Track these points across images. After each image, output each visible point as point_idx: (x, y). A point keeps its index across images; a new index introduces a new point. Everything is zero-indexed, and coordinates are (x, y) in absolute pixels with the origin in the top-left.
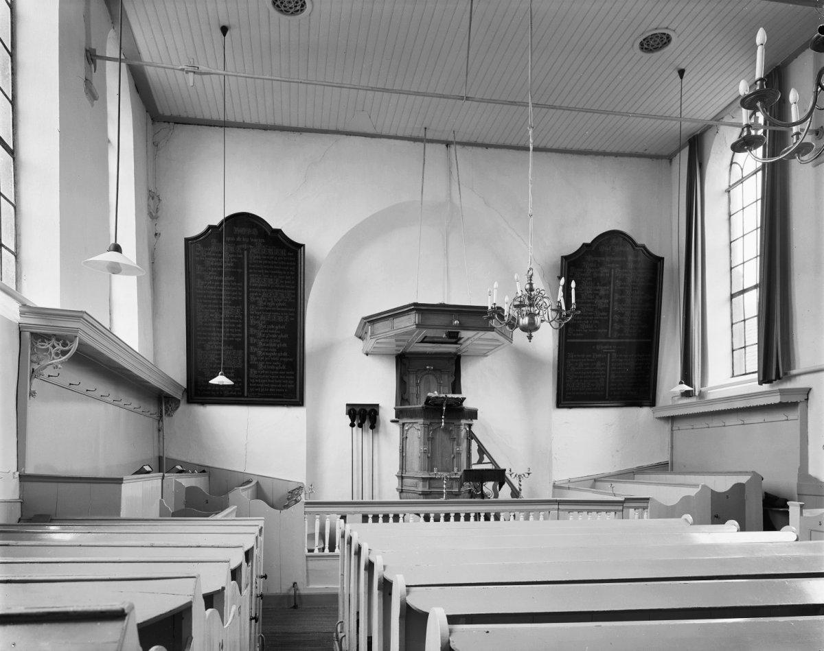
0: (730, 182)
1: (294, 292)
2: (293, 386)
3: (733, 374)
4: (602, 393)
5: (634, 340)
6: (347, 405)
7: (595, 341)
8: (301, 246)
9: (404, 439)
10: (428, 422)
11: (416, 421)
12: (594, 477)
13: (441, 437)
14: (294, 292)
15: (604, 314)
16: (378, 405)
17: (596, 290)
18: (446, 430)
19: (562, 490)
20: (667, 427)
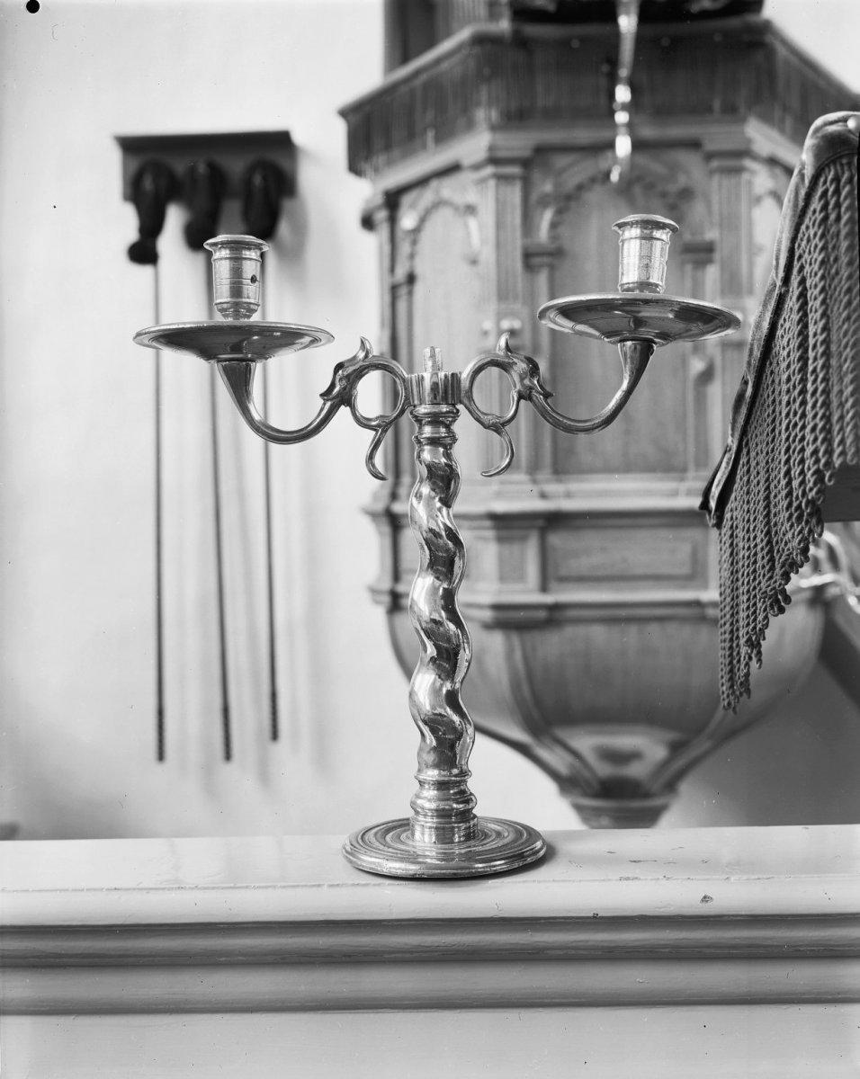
6: (131, 146)
10: (520, 142)
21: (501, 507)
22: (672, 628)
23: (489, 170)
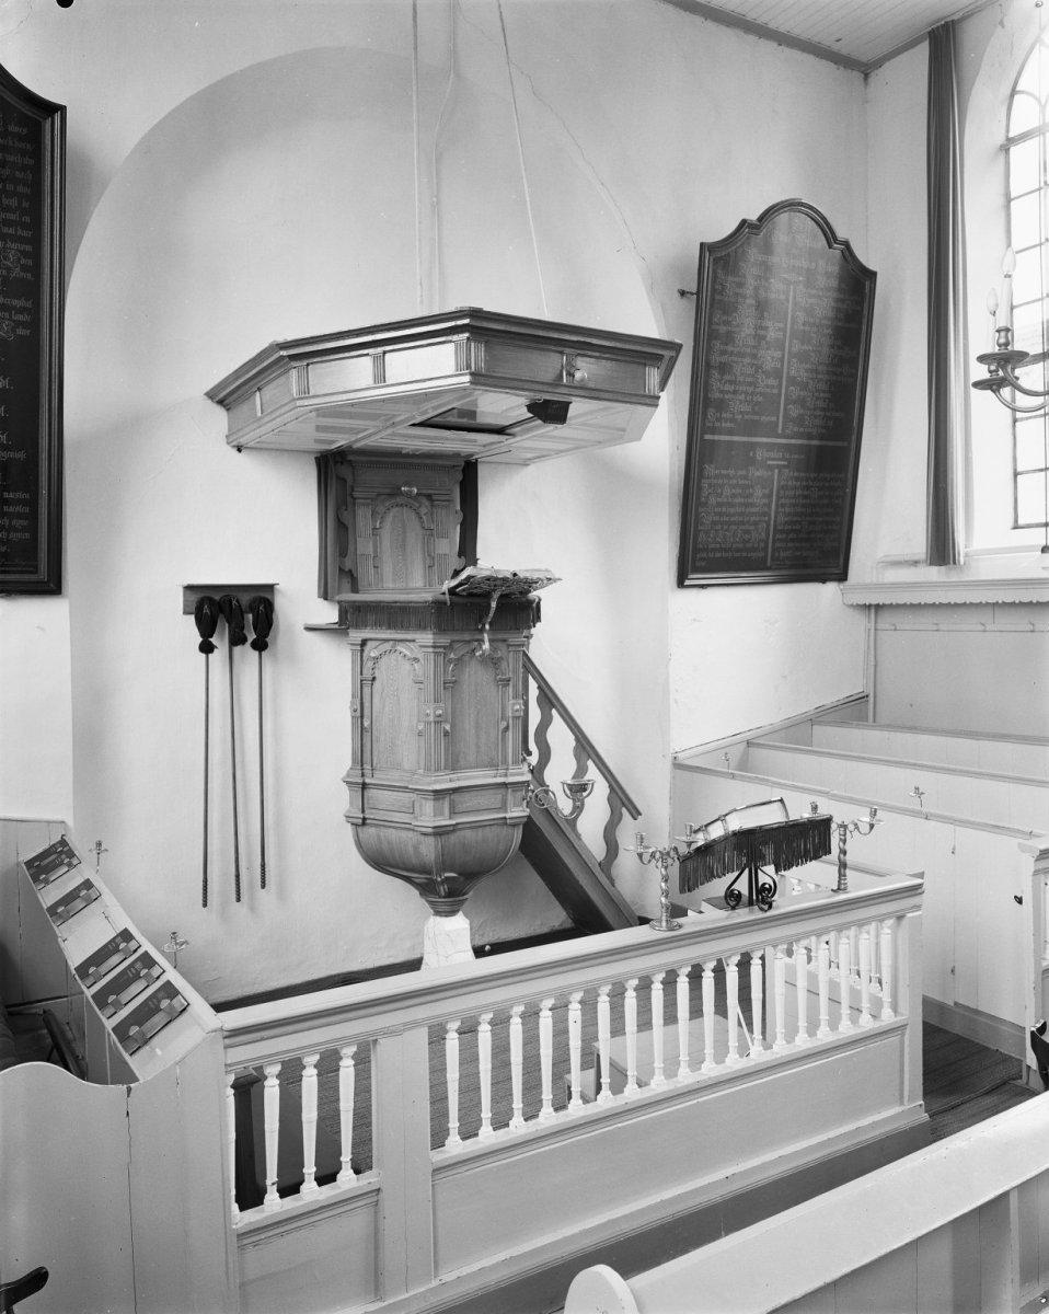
0: (1008, 131)
1: (28, 248)
2: (27, 535)
3: (1016, 521)
4: (761, 554)
5: (800, 442)
6: (189, 588)
7: (830, 443)
8: (53, 110)
9: (364, 684)
10: (445, 640)
11: (409, 636)
12: (748, 736)
13: (475, 677)
14: (28, 248)
15: (771, 381)
16: (270, 588)
17: (761, 328)
18: (493, 662)
19: (706, 777)
20: (861, 622)
21: (438, 787)
22: (493, 828)
23: (431, 650)
